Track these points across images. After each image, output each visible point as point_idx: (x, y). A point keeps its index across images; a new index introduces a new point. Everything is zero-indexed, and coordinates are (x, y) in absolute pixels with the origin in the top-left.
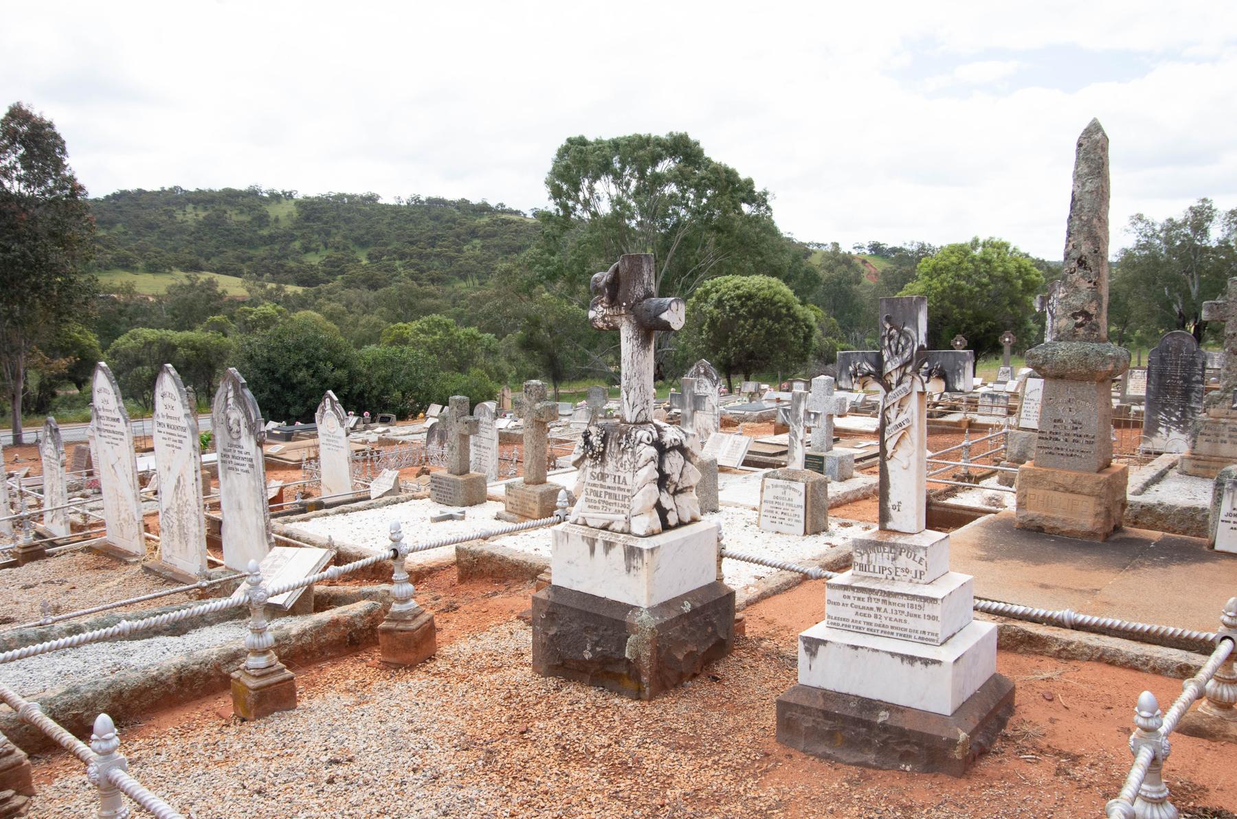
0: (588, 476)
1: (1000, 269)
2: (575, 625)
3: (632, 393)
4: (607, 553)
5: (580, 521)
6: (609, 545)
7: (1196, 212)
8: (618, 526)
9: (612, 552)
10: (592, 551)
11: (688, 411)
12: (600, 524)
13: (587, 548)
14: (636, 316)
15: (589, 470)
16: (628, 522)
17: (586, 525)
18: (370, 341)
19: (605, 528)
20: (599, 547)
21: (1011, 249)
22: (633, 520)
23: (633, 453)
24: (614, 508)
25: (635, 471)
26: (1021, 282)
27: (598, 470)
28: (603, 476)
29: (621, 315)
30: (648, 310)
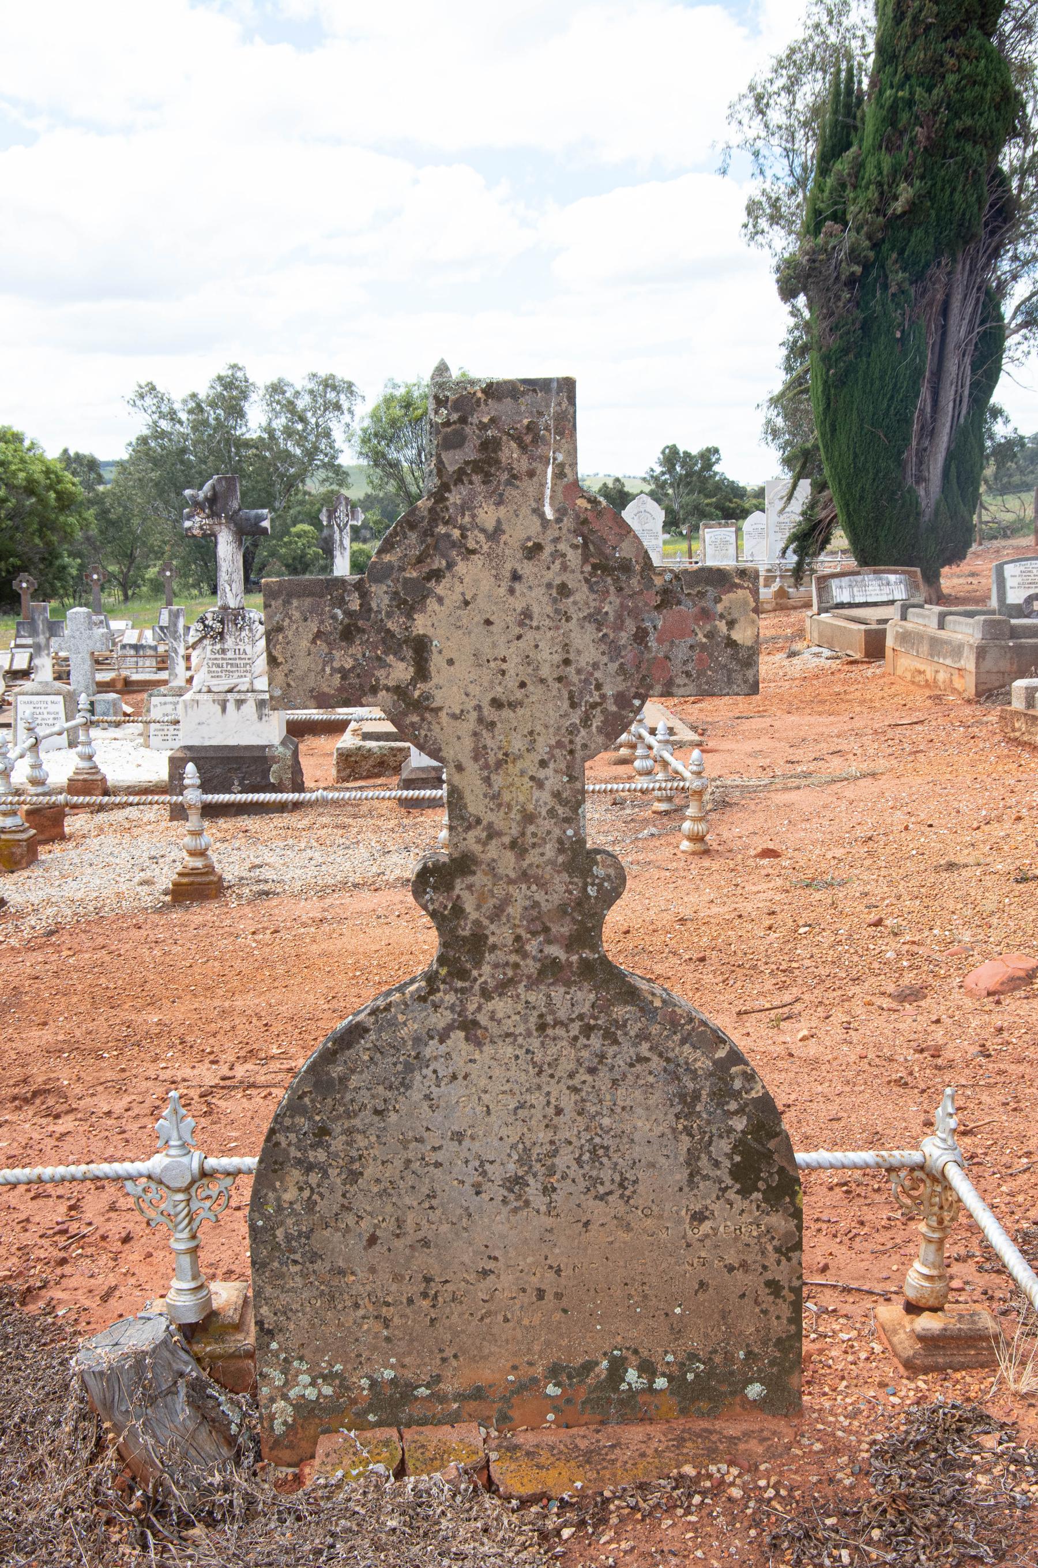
0: (208, 652)
1: (22, 475)
2: (218, 771)
3: (234, 585)
4: (238, 709)
5: (205, 689)
6: (240, 703)
7: (228, 383)
8: (244, 688)
9: (244, 707)
10: (224, 710)
11: (41, 639)
12: (226, 688)
13: (219, 708)
14: (236, 524)
15: (209, 648)
16: (252, 683)
17: (209, 691)
18: (542, 516)
19: (230, 691)
20: (231, 706)
21: (27, 443)
22: (255, 681)
23: (251, 630)
24: (236, 675)
25: (254, 643)
26: (52, 495)
27: (218, 647)
28: (223, 651)
29: (220, 524)
30: (248, 520)
